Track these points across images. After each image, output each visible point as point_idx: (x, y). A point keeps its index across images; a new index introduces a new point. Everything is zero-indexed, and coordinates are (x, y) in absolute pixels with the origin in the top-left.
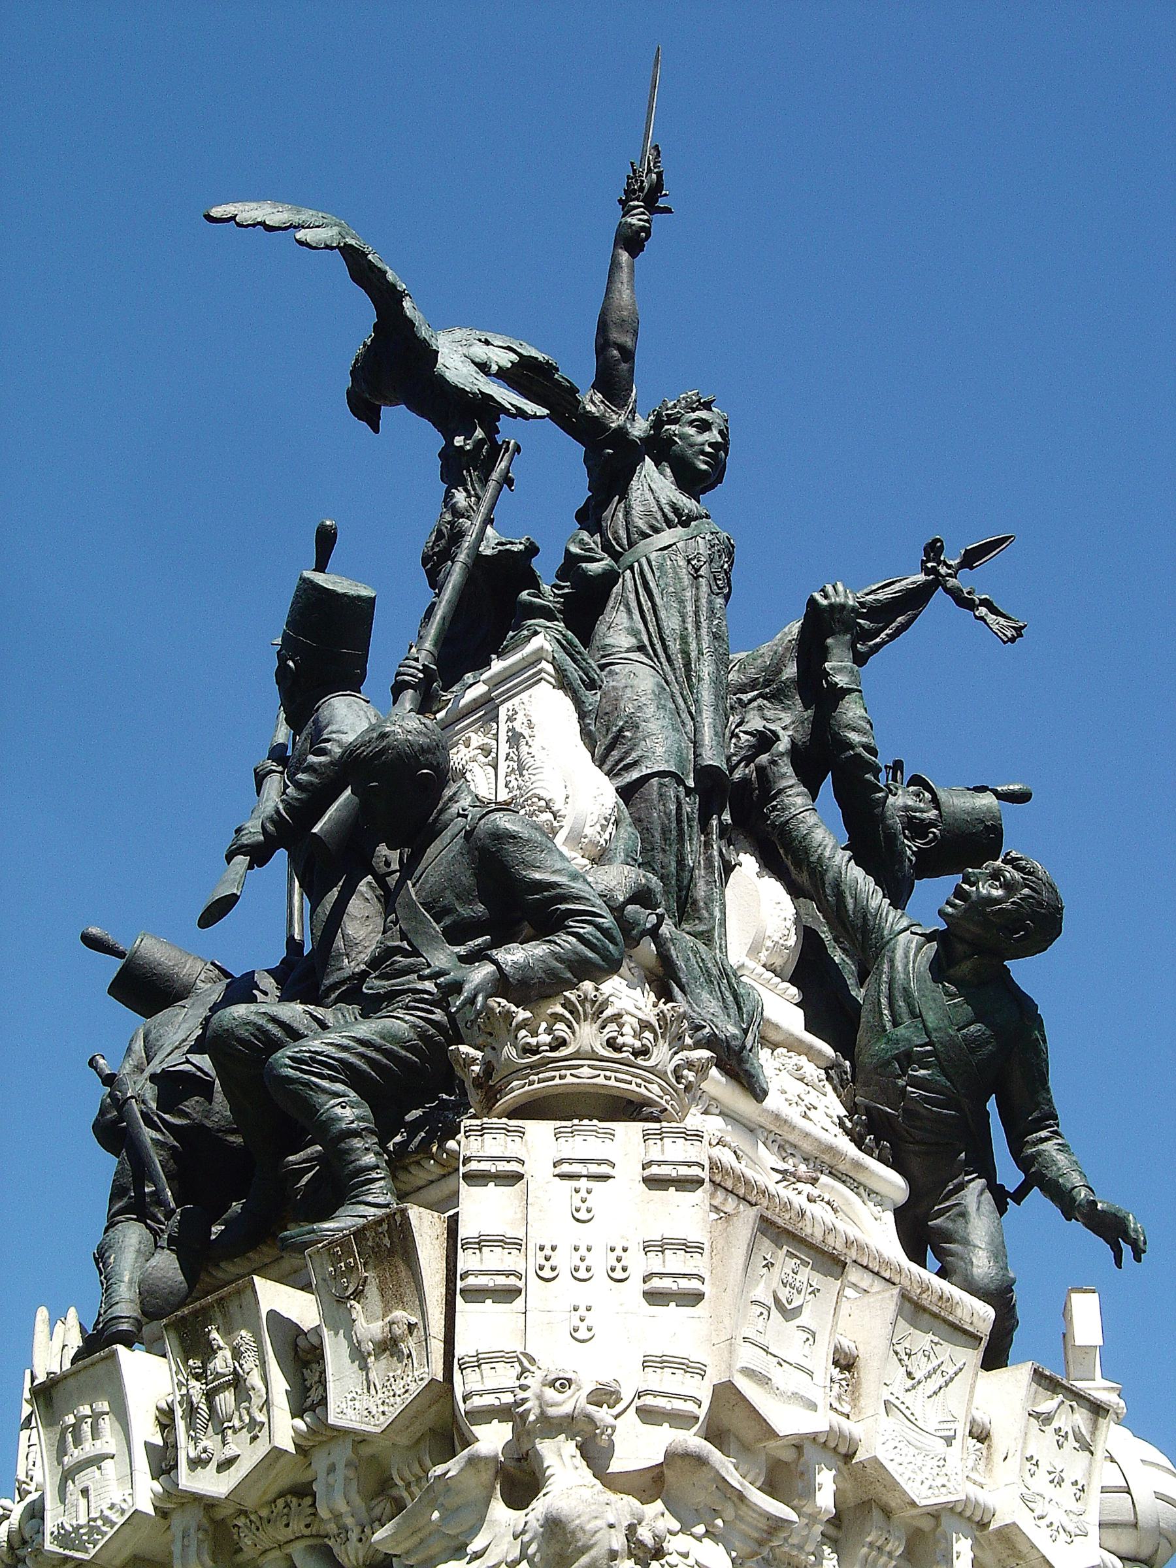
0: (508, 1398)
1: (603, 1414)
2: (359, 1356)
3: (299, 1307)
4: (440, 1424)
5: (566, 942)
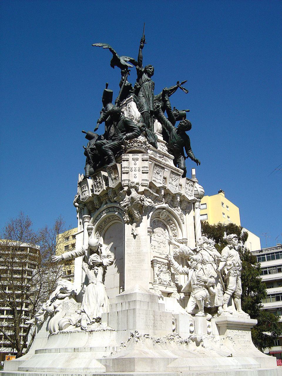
0: (127, 184)
1: (137, 186)
2: (112, 180)
3: (106, 174)
4: (120, 187)
5: (134, 133)
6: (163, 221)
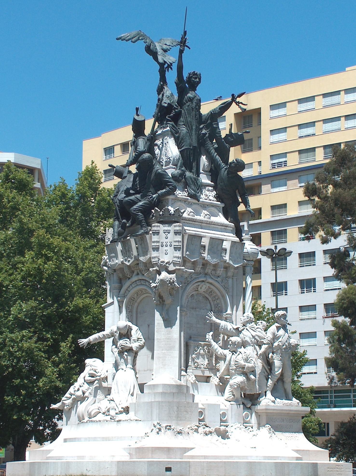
6: (204, 293)
